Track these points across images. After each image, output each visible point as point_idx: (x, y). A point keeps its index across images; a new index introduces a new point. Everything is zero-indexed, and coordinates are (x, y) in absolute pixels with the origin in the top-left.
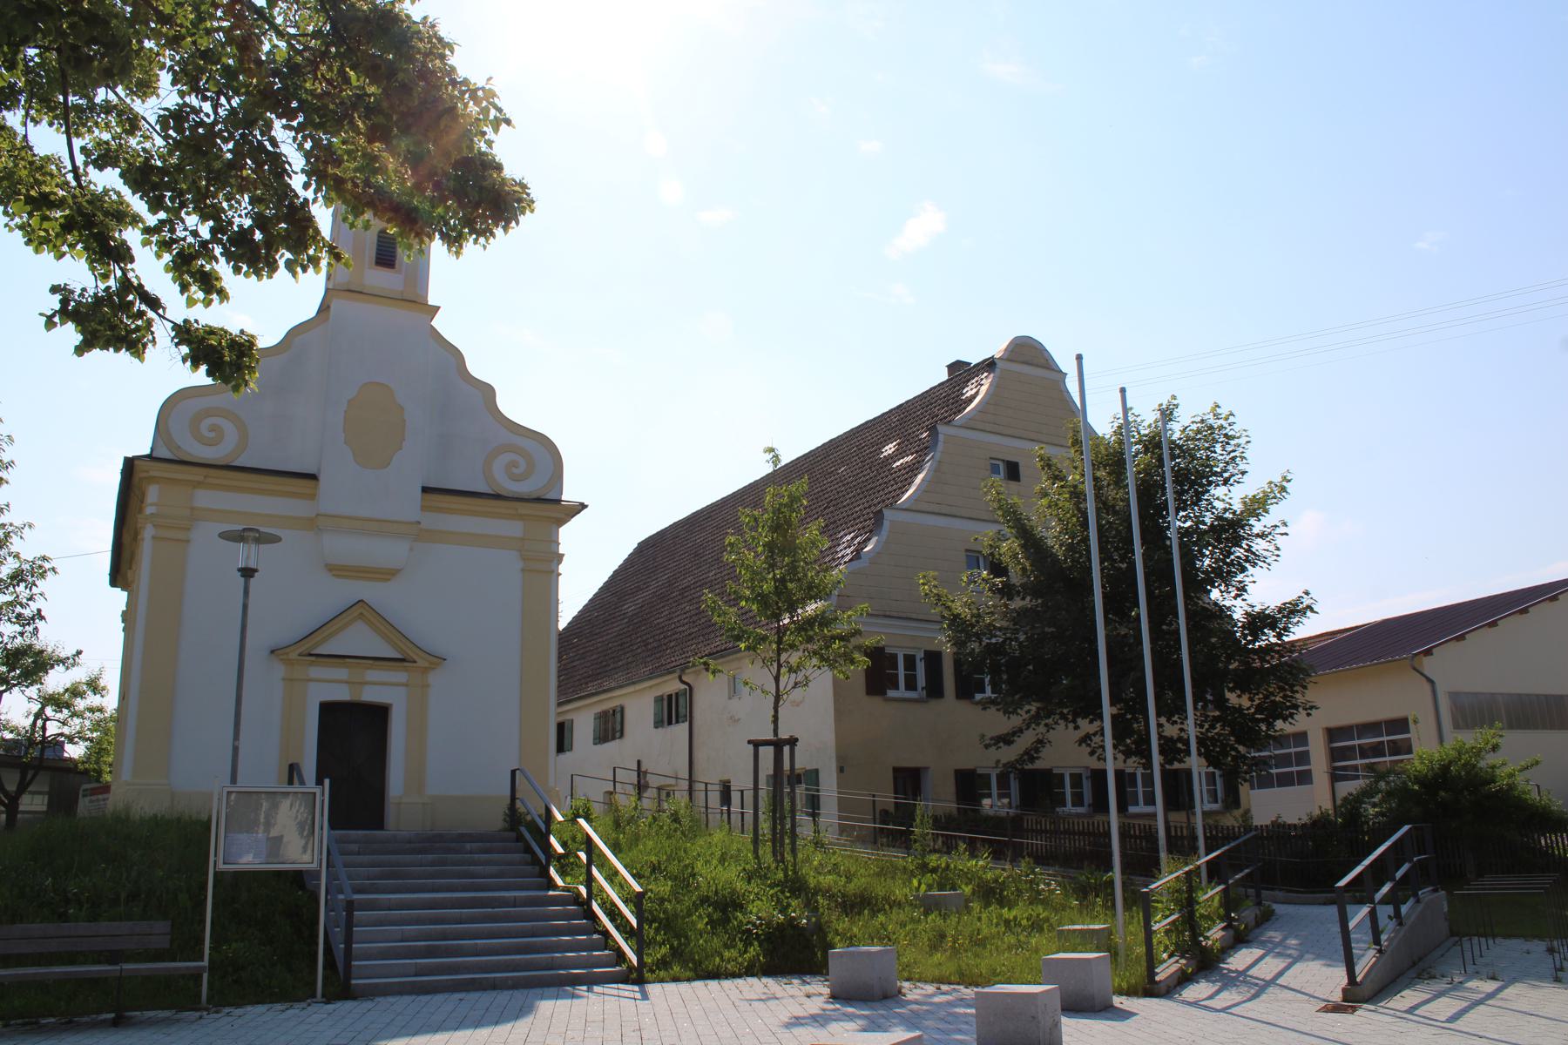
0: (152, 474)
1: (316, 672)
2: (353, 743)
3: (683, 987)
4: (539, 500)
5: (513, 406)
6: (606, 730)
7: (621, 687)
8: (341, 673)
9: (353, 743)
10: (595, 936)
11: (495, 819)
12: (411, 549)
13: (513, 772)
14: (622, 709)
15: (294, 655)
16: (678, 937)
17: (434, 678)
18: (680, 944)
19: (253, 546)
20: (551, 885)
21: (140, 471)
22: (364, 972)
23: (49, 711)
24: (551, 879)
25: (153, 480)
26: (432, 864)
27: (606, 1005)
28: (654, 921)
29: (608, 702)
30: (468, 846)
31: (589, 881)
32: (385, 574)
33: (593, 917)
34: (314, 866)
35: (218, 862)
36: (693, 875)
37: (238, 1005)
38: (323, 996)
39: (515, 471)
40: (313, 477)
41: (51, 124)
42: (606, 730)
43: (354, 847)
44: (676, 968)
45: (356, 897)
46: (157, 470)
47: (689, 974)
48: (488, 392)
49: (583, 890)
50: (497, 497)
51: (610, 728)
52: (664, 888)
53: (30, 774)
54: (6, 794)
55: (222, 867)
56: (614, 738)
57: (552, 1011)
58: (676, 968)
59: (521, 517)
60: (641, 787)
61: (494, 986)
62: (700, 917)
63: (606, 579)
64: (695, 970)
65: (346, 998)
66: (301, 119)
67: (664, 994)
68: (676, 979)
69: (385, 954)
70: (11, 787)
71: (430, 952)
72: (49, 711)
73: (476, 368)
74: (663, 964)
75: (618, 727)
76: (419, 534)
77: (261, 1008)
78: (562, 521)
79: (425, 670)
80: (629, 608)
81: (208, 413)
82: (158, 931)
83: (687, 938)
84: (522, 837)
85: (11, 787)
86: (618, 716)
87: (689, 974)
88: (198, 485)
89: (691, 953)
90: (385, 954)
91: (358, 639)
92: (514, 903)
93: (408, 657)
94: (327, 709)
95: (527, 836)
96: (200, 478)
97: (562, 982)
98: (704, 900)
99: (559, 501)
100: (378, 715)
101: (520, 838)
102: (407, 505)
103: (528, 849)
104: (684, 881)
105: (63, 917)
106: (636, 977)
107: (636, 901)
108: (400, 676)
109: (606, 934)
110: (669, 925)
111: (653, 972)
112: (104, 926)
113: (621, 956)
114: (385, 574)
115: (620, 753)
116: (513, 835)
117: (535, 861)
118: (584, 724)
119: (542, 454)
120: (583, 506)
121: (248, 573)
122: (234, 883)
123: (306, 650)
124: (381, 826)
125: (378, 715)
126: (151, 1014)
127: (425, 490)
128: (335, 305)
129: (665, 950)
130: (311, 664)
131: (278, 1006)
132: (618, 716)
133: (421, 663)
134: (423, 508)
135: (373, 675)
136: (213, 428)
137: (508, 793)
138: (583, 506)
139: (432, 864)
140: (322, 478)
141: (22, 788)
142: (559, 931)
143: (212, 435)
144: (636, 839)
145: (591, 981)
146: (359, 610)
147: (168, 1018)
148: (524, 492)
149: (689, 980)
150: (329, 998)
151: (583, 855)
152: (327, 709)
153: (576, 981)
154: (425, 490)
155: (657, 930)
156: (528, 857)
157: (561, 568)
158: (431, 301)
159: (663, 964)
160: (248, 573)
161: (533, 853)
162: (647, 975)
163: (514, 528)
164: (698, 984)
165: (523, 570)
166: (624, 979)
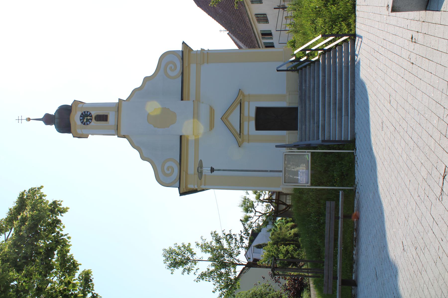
0: (184, 187)
1: (245, 132)
2: (268, 119)
3: (358, 20)
4: (182, 59)
5: (150, 70)
6: (264, 20)
7: (248, 16)
8: (246, 124)
9: (268, 119)
10: (337, 48)
11: (295, 75)
12: (203, 103)
13: (278, 71)
14: (256, 15)
15: (240, 140)
16: (339, 18)
17: (246, 93)
18: (342, 18)
19: (204, 168)
20: (318, 60)
21: (184, 190)
22: (345, 136)
23: (261, 198)
24: (316, 61)
25: (186, 187)
26: (310, 101)
27: (364, 52)
28: (332, 27)
29: (254, 20)
30: (304, 88)
31: (317, 50)
32: (212, 111)
33: (330, 49)
34: (310, 154)
35: (308, 186)
36: (316, 8)
37: (355, 178)
38: (353, 150)
39: (173, 68)
40: (181, 137)
41: (68, 251)
42: (264, 20)
43: (303, 127)
44: (351, 21)
45: (320, 139)
46: (183, 186)
47: (353, 16)
48: (146, 79)
49: (320, 52)
50: (182, 73)
51: (263, 18)
52: (320, 21)
53: (280, 202)
54: (286, 208)
55: (309, 184)
56: (267, 17)
57: (365, 73)
58: (351, 21)
59: (189, 65)
60: (284, 8)
61: (353, 89)
62: (331, 8)
63: (211, 18)
64: (352, 13)
65: (355, 142)
66: (12, 284)
67: (360, 28)
68: (355, 21)
69: (340, 125)
70: (284, 207)
71: (340, 109)
72: (261, 198)
73: (138, 84)
74: (349, 25)
75: (262, 16)
76: (197, 100)
77: (356, 171)
78: (190, 50)
79: (244, 96)
80: (220, 11)
81: (163, 171)
82: (330, 205)
83: (339, 15)
84: (299, 67)
85: (284, 207)
86: (258, 16)
87: (353, 16)
88: (187, 173)
89: (345, 13)
90: (340, 125)
91: (234, 118)
92: (324, 76)
93: (240, 102)
94: (258, 128)
95: (300, 67)
96: (185, 172)
97: (353, 67)
98: (325, 5)
99: (182, 51)
100: (259, 110)
101: (301, 69)
102: (188, 105)
103: (305, 67)
104: (318, 13)
105: (324, 223)
106: (353, 36)
107: (325, 36)
108: (246, 104)
109: (337, 45)
110: (334, 22)
111: (351, 30)
112: (327, 221)
113: (345, 41)
114: (212, 111)
115: (272, 15)
116: (300, 71)
117: (309, 65)
118: (261, 27)
119: (166, 59)
120: (183, 43)
121: (212, 170)
122: (315, 180)
123: (239, 136)
124: (297, 109)
125: (259, 110)
126: (355, 205)
127: (182, 99)
128: (122, 133)
129: (343, 24)
130: (243, 134)
131: (356, 165)
132: (258, 16)
133: (241, 98)
134: (188, 100)
135: (246, 113)
136: (168, 169)
137: (285, 73)
138: (183, 43)
139: (310, 101)
140: (181, 134)
141: (284, 204)
142: (335, 62)
143: (170, 169)
144: (302, 25)
145: (354, 54)
146: (224, 119)
147: (357, 201)
148: (182, 64)
149: (355, 16)
150: (354, 148)
151: (307, 52)
152: (258, 128)
153: (353, 60)
154: (182, 99)
155: (336, 25)
156: (308, 67)
157: (206, 49)
158: (118, 101)
159: (349, 25)
160: (212, 170)
161: (307, 65)
162: (352, 32)
163: (193, 67)
164: (357, 13)
165: (208, 63)
166: (354, 41)
